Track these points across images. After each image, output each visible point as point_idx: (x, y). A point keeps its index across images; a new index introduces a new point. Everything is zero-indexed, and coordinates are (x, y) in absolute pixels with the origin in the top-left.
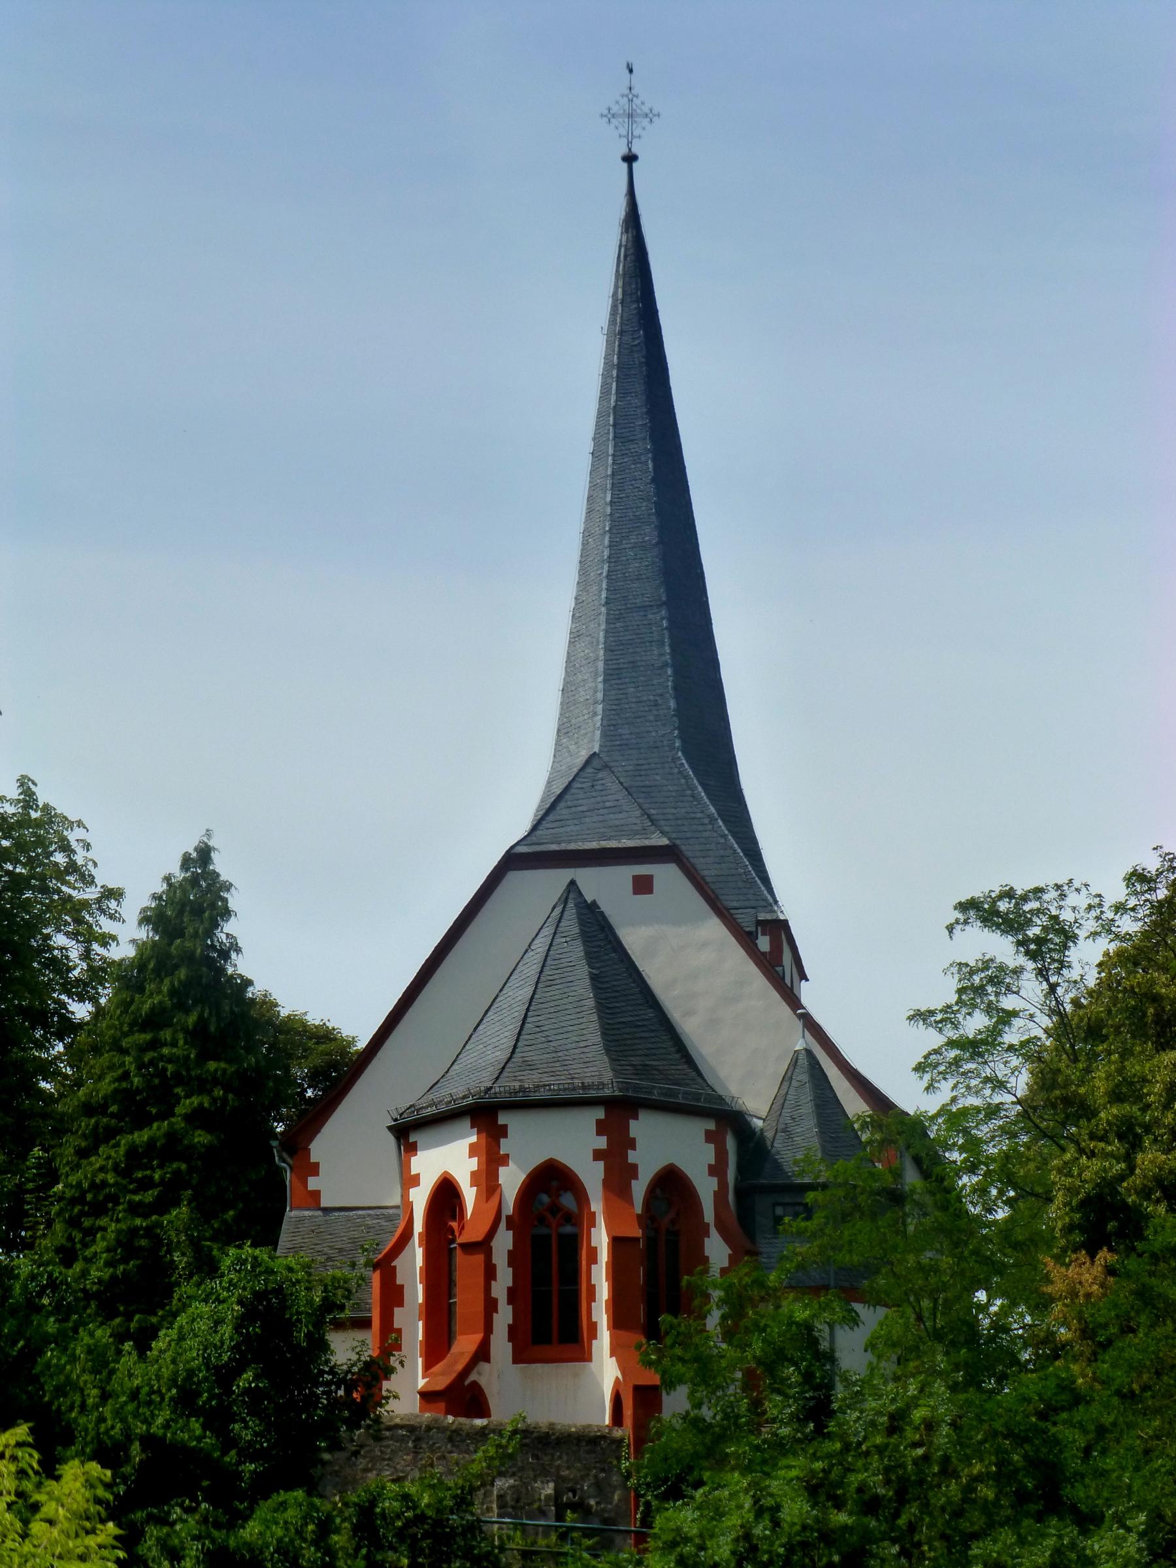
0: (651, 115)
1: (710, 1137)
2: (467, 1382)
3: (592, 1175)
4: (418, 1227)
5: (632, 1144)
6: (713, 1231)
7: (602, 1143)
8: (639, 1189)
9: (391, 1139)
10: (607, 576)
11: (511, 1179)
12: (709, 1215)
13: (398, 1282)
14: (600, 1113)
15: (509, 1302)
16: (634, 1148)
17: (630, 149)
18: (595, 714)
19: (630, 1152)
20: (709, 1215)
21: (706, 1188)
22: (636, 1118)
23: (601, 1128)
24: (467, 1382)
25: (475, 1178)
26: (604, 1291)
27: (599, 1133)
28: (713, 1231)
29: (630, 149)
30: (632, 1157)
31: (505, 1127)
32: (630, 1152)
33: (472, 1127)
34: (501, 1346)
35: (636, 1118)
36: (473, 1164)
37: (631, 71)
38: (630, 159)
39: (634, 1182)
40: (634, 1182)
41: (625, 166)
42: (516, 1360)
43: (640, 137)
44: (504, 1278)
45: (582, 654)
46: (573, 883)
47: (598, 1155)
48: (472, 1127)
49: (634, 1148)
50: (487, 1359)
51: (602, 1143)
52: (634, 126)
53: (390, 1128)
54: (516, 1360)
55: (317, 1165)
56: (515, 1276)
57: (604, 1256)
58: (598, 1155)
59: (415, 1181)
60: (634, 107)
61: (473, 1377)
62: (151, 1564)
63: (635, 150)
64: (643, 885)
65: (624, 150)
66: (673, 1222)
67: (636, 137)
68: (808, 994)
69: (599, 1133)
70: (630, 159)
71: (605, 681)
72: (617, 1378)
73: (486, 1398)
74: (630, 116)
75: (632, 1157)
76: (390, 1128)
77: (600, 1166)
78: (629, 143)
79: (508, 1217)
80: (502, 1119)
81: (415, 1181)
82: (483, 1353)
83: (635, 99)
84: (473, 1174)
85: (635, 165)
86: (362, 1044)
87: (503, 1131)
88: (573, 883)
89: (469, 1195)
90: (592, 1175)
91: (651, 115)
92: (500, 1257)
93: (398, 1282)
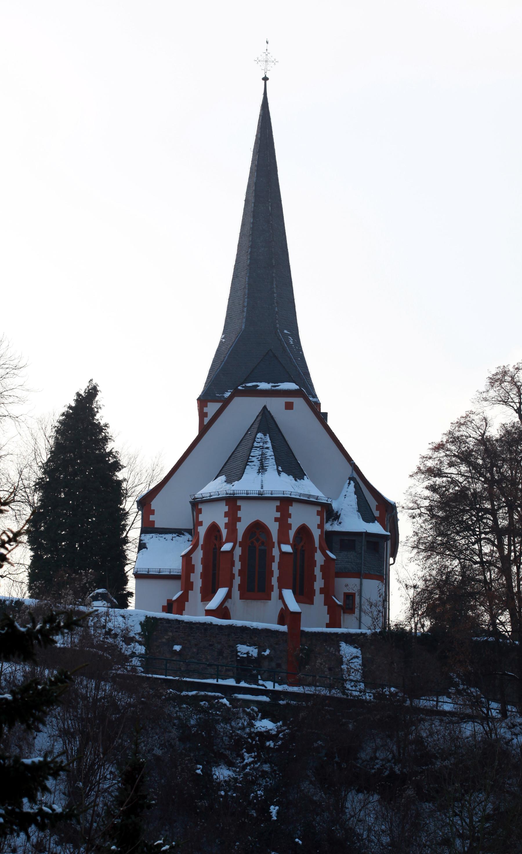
0: (275, 62)
1: (319, 513)
2: (223, 607)
3: (274, 528)
5: (290, 516)
6: (318, 550)
7: (278, 515)
9: (190, 506)
10: (250, 253)
11: (241, 528)
12: (317, 544)
13: (193, 563)
15: (234, 574)
16: (290, 518)
18: (243, 311)
19: (289, 519)
20: (317, 544)
22: (292, 506)
23: (278, 509)
24: (223, 607)
25: (227, 526)
26: (276, 573)
27: (277, 511)
28: (318, 550)
30: (290, 521)
31: (240, 506)
32: (289, 519)
33: (226, 505)
34: (236, 593)
35: (292, 506)
36: (226, 520)
37: (267, 42)
38: (265, 79)
42: (241, 598)
44: (238, 566)
45: (238, 285)
46: (265, 407)
47: (276, 520)
48: (226, 505)
49: (290, 518)
50: (230, 598)
51: (278, 515)
52: (268, 66)
53: (190, 502)
54: (241, 598)
55: (154, 510)
56: (242, 565)
57: (277, 559)
58: (276, 520)
60: (268, 58)
61: (226, 604)
62: (204, 702)
64: (289, 406)
66: (302, 546)
69: (277, 511)
70: (265, 79)
71: (248, 298)
72: (282, 608)
73: (229, 613)
74: (266, 61)
75: (290, 521)
76: (190, 502)
79: (239, 542)
80: (239, 503)
81: (201, 524)
83: (274, 63)
84: (226, 524)
85: (267, 81)
87: (239, 508)
88: (265, 407)
90: (274, 528)
91: (275, 62)
92: (236, 558)
93: (193, 563)
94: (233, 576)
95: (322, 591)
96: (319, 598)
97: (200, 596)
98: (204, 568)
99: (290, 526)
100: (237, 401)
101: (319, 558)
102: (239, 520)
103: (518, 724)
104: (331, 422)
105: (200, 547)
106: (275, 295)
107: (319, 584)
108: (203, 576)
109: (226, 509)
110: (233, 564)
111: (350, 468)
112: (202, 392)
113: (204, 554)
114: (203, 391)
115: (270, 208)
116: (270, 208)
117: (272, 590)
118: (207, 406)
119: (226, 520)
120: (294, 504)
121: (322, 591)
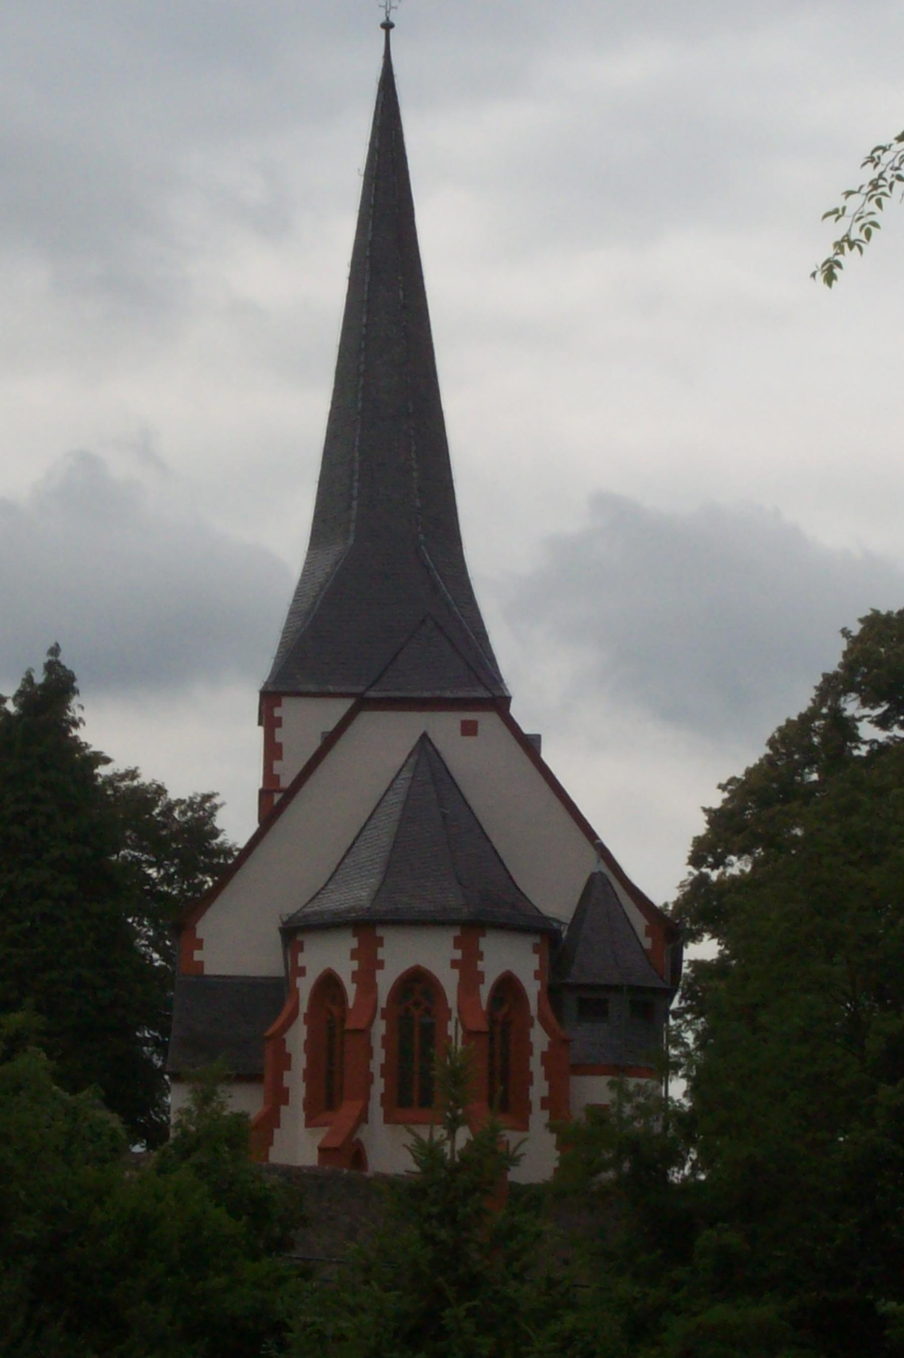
4: (304, 1007)
5: (480, 956)
6: (536, 1022)
7: (458, 954)
8: (485, 991)
11: (385, 980)
14: (456, 932)
15: (372, 1074)
17: (388, 19)
21: (532, 989)
23: (458, 944)
25: (355, 976)
29: (388, 19)
34: (376, 1111)
36: (355, 965)
38: (388, 26)
39: (481, 986)
40: (481, 986)
41: (383, 32)
42: (386, 1121)
43: (396, 8)
46: (424, 737)
47: (454, 964)
50: (366, 1121)
51: (458, 954)
58: (454, 964)
59: (302, 972)
61: (356, 1136)
63: (392, 19)
64: (469, 729)
65: (383, 19)
67: (393, 8)
68: (515, 711)
70: (388, 26)
75: (481, 965)
77: (456, 973)
78: (387, 12)
79: (383, 1009)
80: (380, 932)
81: (302, 972)
82: (363, 1118)
84: (354, 973)
85: (392, 32)
86: (242, 844)
87: (380, 942)
88: (424, 737)
89: (351, 990)
94: (370, 1079)
95: (545, 1103)
96: (539, 1117)
97: (302, 1116)
98: (311, 1061)
99: (480, 977)
100: (367, 720)
101: (539, 1038)
102: (380, 965)
103: (673, 1056)
104: (547, 755)
105: (301, 1017)
106: (415, 474)
107: (539, 1089)
108: (309, 1075)
109: (353, 943)
110: (370, 1053)
111: (592, 854)
112: (270, 677)
113: (311, 1032)
114: (272, 672)
115: (401, 293)
116: (401, 293)
117: (384, 1038)
118: (279, 705)
119: (355, 965)
120: (285, 701)
121: (545, 1103)
